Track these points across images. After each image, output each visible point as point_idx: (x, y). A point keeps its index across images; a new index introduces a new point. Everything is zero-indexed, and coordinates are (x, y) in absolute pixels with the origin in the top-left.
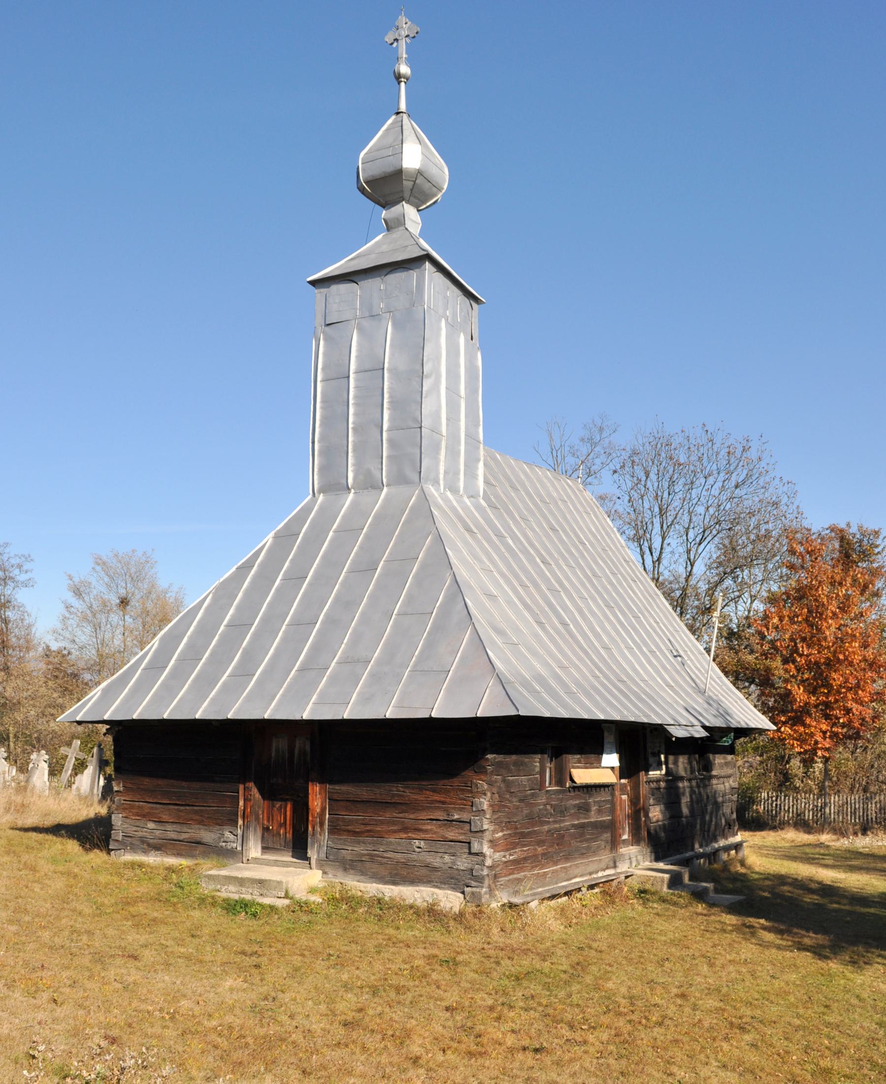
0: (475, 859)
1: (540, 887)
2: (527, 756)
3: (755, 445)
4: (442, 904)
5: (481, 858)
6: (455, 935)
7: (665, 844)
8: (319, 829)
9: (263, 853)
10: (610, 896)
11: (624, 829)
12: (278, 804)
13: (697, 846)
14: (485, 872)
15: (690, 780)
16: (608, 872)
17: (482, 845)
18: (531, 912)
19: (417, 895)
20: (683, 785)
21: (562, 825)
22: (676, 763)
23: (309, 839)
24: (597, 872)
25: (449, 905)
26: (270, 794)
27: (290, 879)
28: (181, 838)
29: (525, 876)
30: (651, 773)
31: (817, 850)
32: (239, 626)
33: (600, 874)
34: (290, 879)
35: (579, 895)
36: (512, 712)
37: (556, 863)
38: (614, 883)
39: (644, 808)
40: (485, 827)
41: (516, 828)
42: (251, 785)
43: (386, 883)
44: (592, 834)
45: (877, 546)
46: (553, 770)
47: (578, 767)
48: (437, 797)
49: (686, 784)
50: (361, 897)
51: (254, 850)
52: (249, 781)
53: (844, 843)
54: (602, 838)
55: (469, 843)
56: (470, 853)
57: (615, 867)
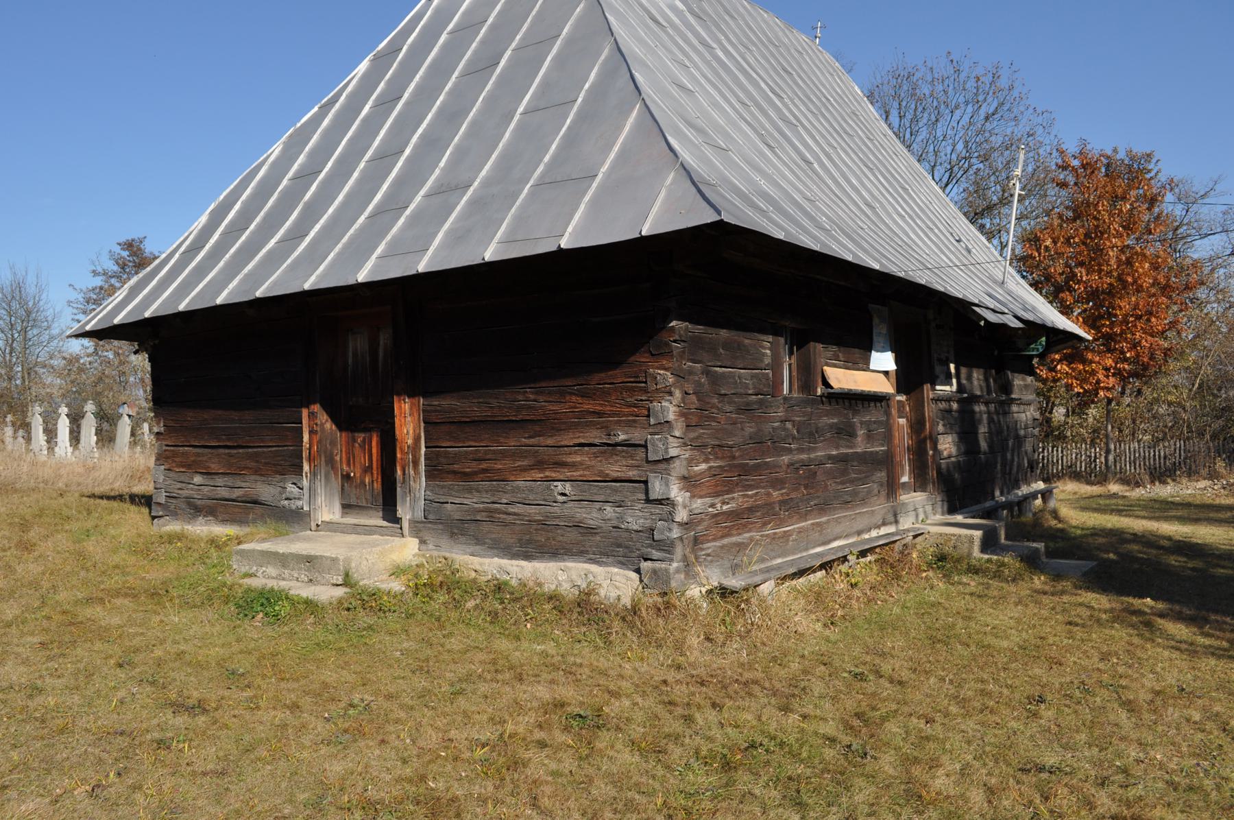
0: (657, 509)
1: (779, 557)
2: (748, 334)
3: (1005, 74)
4: (602, 593)
5: (668, 508)
6: (618, 650)
7: (962, 490)
8: (412, 472)
9: (344, 514)
10: (892, 567)
11: (902, 467)
12: (360, 437)
13: (997, 493)
14: (676, 533)
15: (987, 404)
16: (884, 531)
17: (667, 485)
18: (762, 600)
19: (562, 577)
20: (979, 408)
21: (812, 456)
22: (969, 378)
23: (398, 489)
24: (869, 530)
25: (613, 594)
26: (347, 421)
27: (354, 554)
28: (234, 496)
29: (751, 539)
30: (938, 387)
31: (1114, 501)
32: (306, 176)
33: (874, 533)
34: (354, 554)
35: (844, 568)
36: (709, 217)
37: (804, 517)
38: (898, 547)
39: (931, 437)
40: (673, 452)
41: (734, 458)
42: (316, 408)
43: (514, 556)
44: (860, 472)
45: (1149, 171)
46: (794, 367)
47: (835, 366)
48: (588, 406)
49: (983, 408)
50: (474, 581)
51: (328, 510)
52: (314, 403)
53: (1138, 493)
54: (874, 478)
55: (646, 482)
56: (648, 501)
57: (896, 522)
